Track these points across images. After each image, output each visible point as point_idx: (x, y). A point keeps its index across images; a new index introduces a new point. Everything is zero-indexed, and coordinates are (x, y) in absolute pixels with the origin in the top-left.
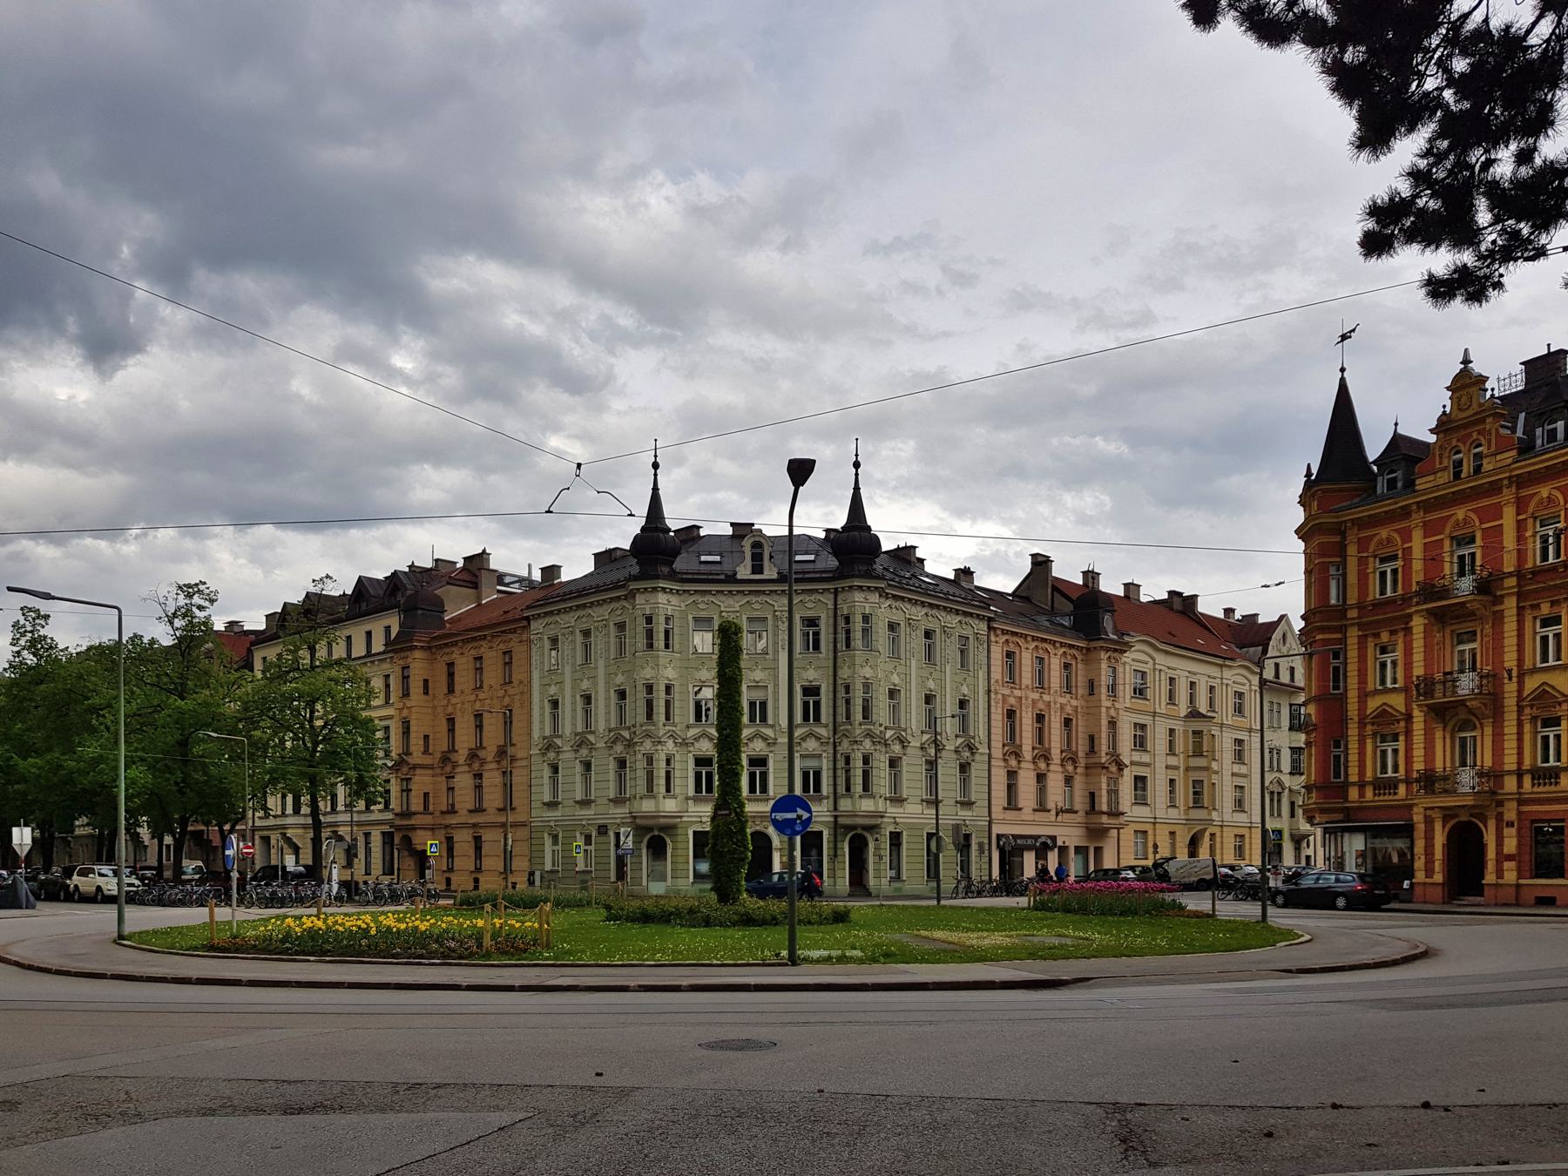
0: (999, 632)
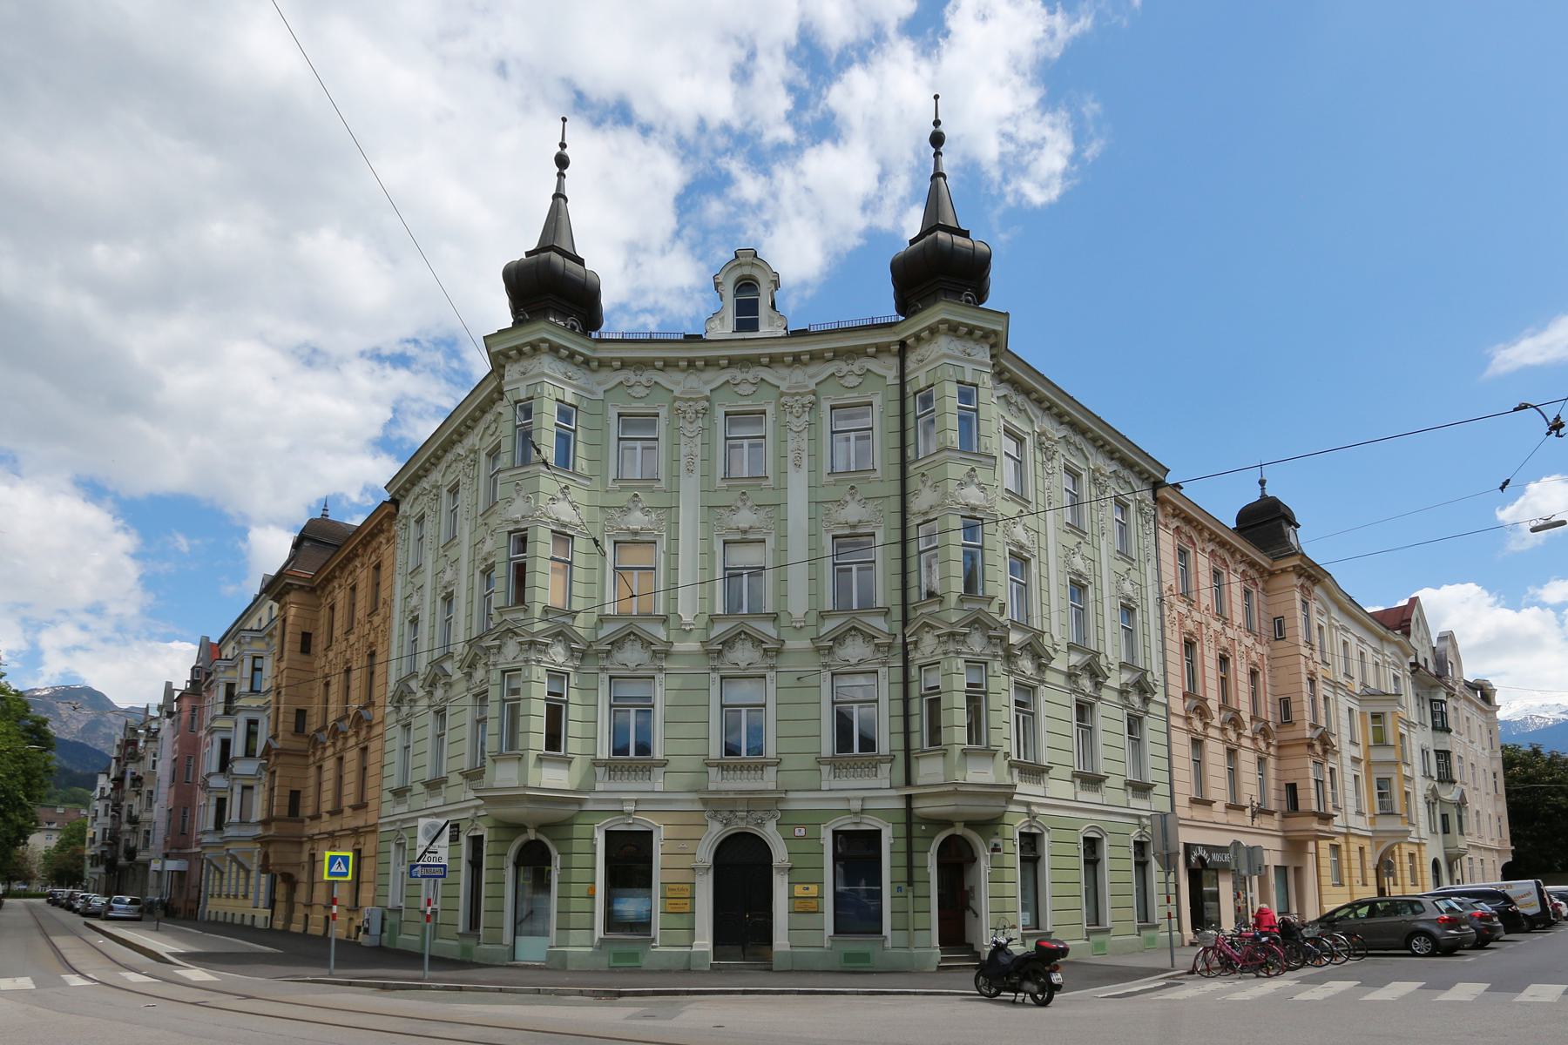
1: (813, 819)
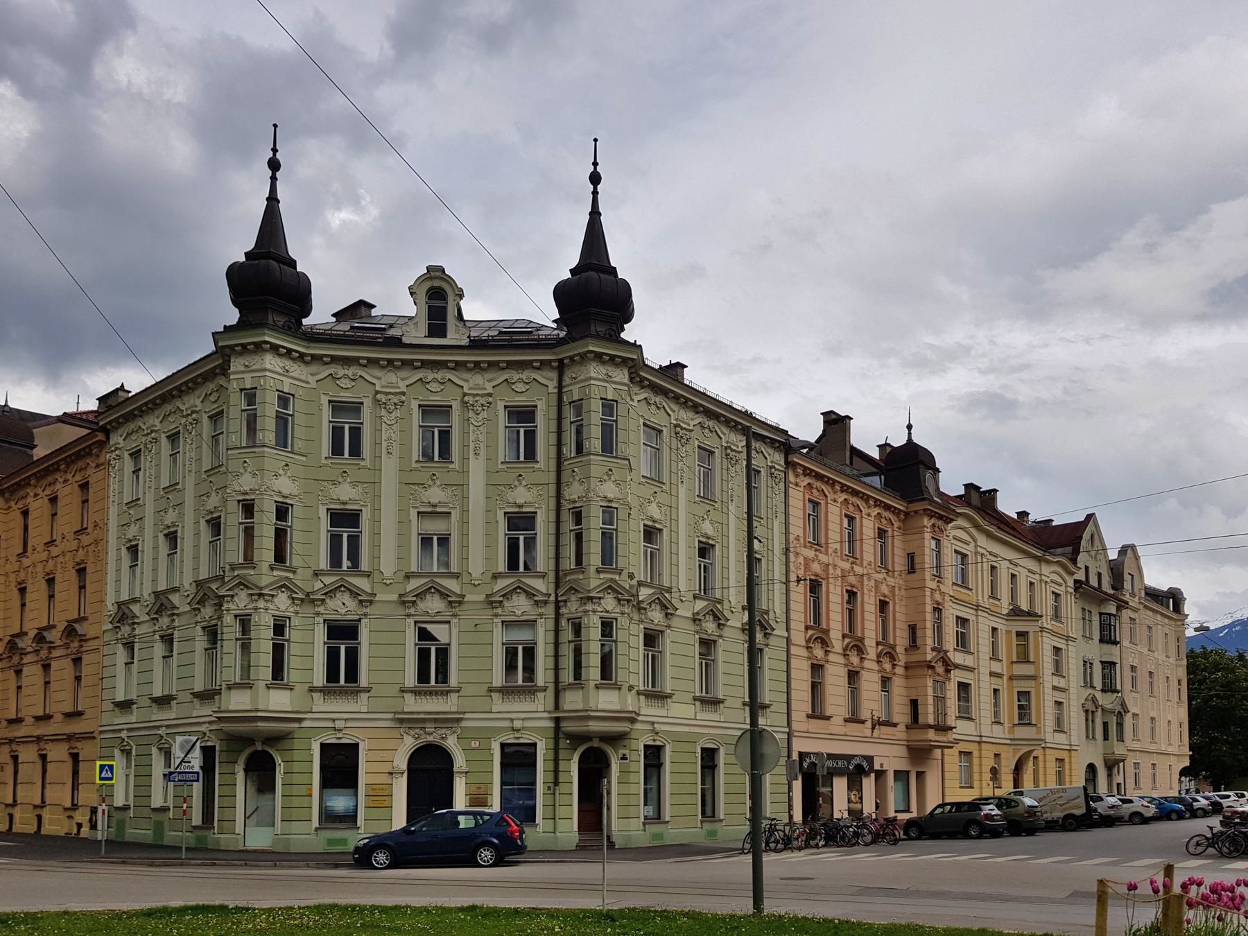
0: (800, 471)
1: (485, 735)
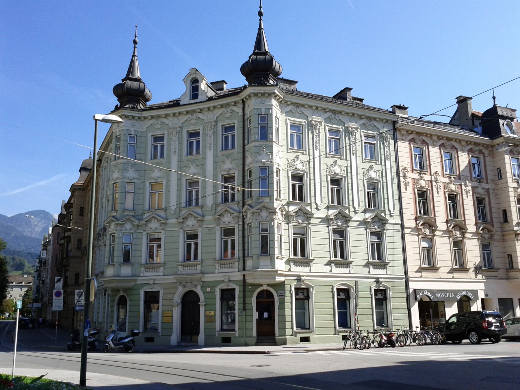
1: (213, 284)
